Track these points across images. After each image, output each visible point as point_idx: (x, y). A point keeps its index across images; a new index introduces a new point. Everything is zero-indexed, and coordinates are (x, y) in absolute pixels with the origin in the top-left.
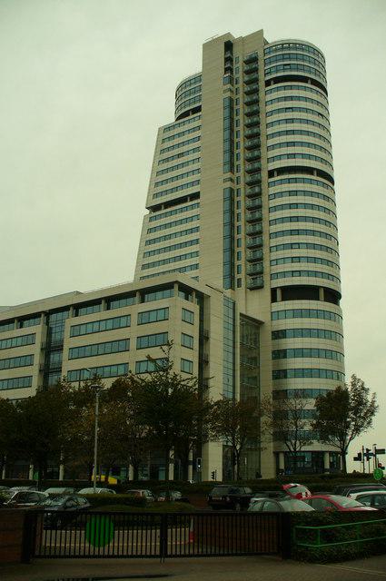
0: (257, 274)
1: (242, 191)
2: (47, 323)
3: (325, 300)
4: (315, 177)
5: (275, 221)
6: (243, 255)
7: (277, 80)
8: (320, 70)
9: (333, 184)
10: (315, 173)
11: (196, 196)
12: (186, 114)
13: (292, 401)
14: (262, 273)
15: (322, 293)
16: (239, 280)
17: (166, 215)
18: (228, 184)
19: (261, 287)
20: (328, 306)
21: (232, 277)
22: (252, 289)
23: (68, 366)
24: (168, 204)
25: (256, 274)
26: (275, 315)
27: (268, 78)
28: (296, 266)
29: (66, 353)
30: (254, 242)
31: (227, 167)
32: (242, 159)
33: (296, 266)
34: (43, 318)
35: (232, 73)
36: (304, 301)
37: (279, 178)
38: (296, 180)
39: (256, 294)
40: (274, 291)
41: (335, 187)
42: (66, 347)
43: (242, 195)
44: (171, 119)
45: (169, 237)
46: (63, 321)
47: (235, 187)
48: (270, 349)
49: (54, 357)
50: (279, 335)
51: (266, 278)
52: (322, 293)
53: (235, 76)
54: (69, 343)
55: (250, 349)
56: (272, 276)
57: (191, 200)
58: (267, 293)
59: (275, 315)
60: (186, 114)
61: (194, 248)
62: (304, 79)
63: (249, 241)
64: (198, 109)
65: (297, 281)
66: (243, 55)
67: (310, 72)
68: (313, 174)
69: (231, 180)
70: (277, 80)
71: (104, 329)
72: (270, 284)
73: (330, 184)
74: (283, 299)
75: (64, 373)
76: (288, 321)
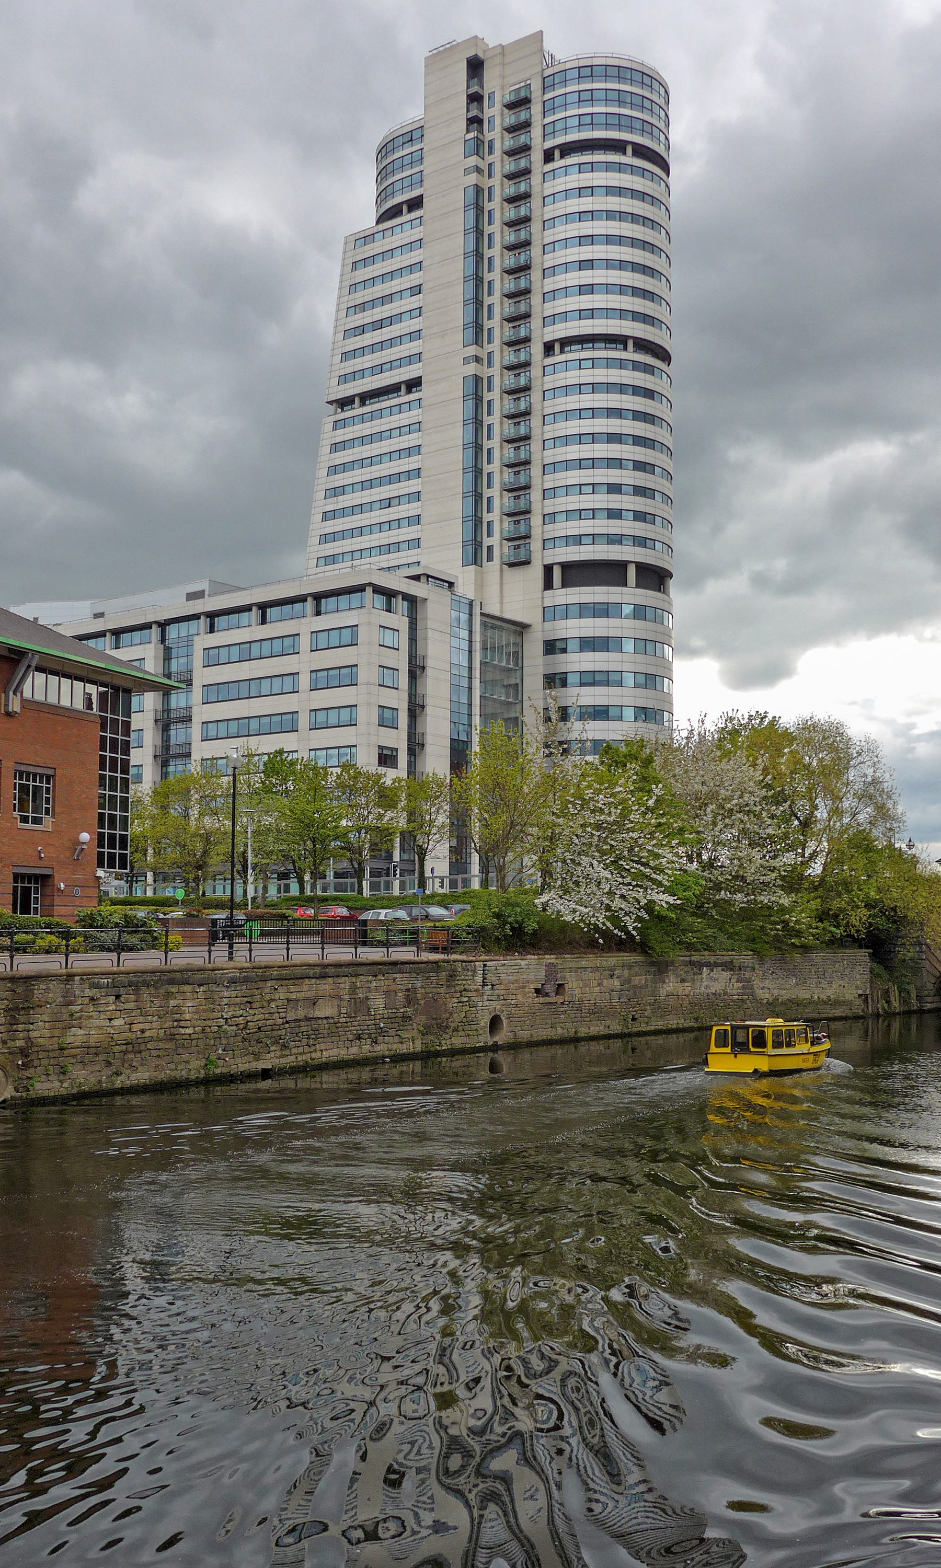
0: (520, 489)
1: (497, 381)
2: (163, 640)
3: (638, 586)
4: (628, 159)
5: (555, 466)
6: (496, 479)
7: (567, 149)
8: (654, 121)
9: (668, 175)
10: (629, 149)
11: (414, 384)
12: (395, 212)
13: (578, 725)
14: (528, 537)
15: (632, 572)
16: (490, 548)
17: (362, 418)
18: (473, 178)
19: (527, 563)
20: (646, 596)
21: (477, 545)
22: (511, 565)
23: (201, 750)
24: (365, 398)
25: (520, 539)
26: (549, 613)
27: (549, 144)
28: (587, 301)
29: (196, 731)
30: (517, 308)
31: (471, 332)
32: (498, 129)
33: (587, 301)
34: (155, 632)
35: (481, 131)
36: (597, 589)
37: (562, 162)
38: (592, 167)
39: (518, 572)
40: (548, 569)
41: (672, 180)
42: (197, 719)
43: (497, 198)
44: (367, 219)
45: (372, 461)
46: (189, 642)
47: (485, 372)
48: (541, 671)
49: (177, 734)
50: (552, 647)
51: (535, 545)
52: (632, 572)
53: (488, 136)
54: (202, 676)
55: (510, 670)
56: (547, 321)
57: (410, 210)
58: (536, 573)
59: (549, 613)
60: (395, 212)
61: (412, 486)
62: (618, 146)
63: (508, 476)
64: (416, 204)
65: (586, 553)
66: (503, 88)
67: (631, 129)
68: (625, 153)
69: (478, 360)
70: (567, 149)
71: (258, 655)
72: (540, 557)
73: (664, 175)
74: (564, 585)
75: (194, 767)
76: (571, 623)
